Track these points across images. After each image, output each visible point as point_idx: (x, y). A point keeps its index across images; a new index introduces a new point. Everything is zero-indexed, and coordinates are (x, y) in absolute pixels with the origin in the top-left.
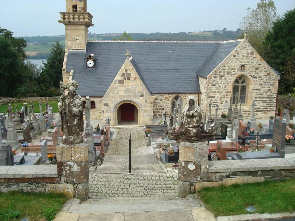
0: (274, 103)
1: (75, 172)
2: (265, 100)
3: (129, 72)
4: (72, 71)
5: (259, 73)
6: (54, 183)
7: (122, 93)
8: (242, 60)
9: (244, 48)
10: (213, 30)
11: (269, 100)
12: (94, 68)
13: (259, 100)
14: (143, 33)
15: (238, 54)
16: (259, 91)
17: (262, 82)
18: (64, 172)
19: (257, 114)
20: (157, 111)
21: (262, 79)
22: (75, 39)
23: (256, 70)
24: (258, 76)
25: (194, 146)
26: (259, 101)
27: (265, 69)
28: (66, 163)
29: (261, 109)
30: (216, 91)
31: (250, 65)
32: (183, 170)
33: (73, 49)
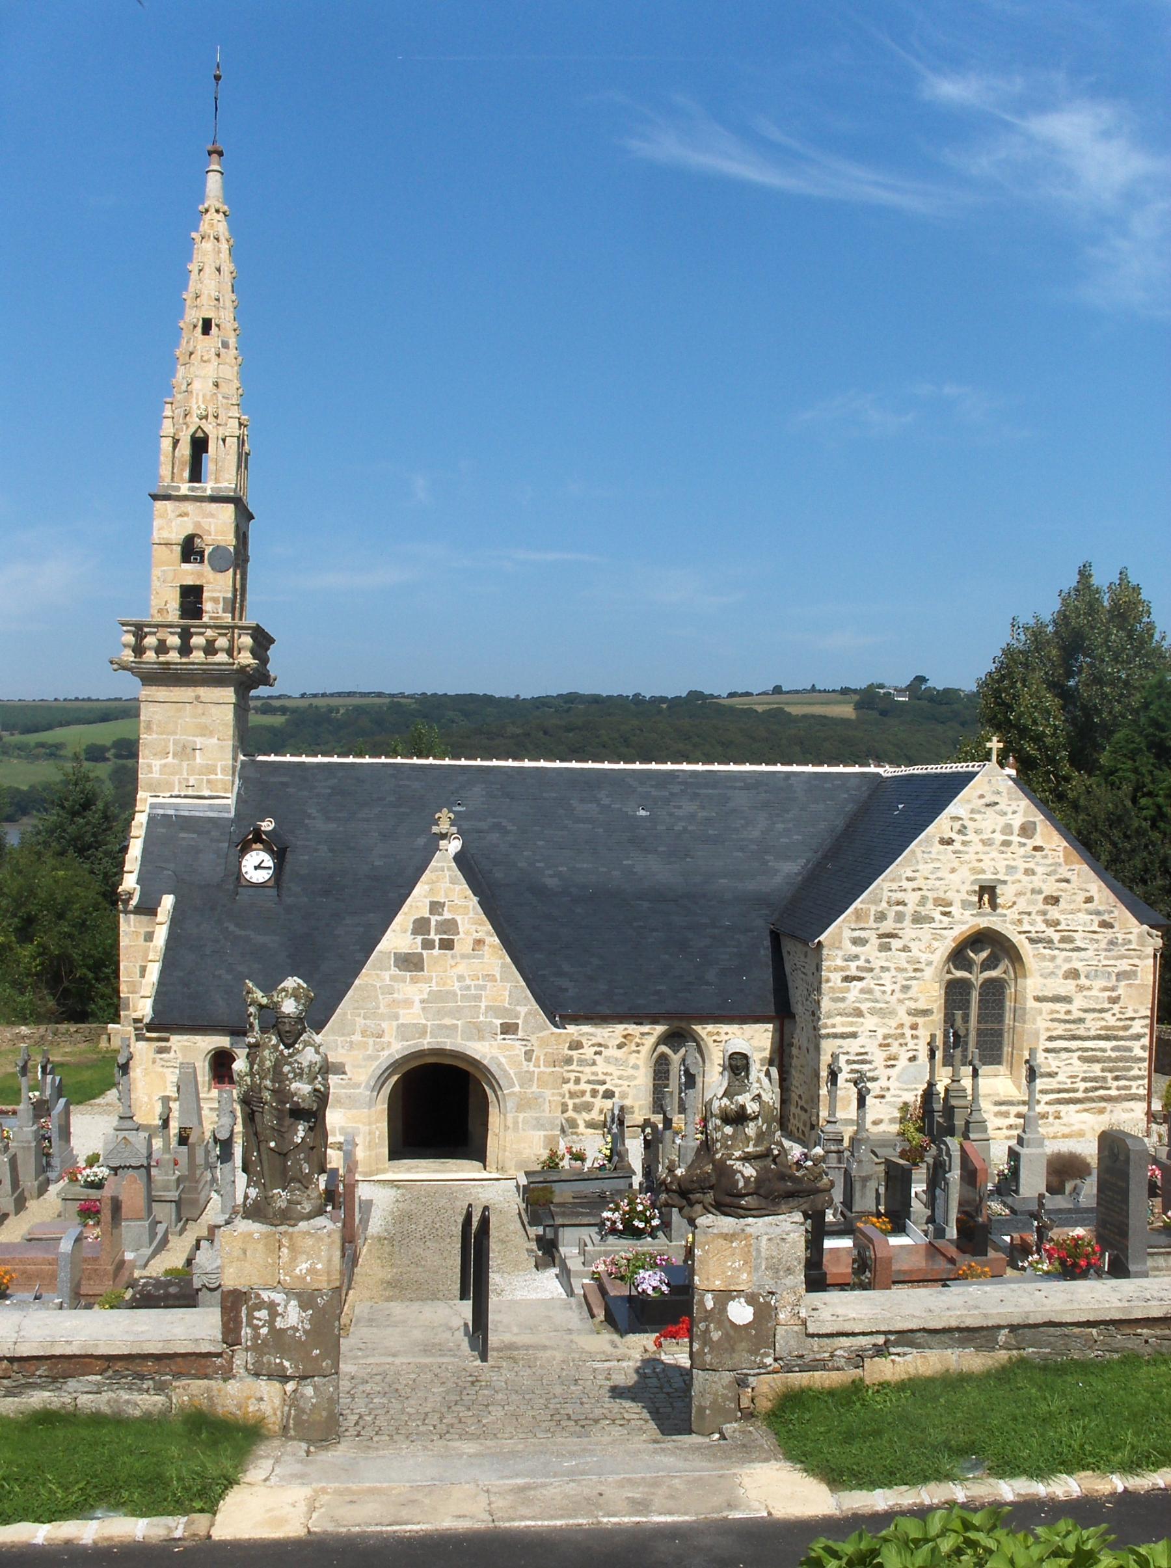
0: (1141, 1060)
1: (290, 1332)
2: (1093, 1050)
3: (447, 915)
4: (168, 901)
5: (1063, 923)
6: (206, 1377)
7: (413, 1015)
8: (981, 860)
9: (987, 805)
10: (859, 682)
11: (1113, 1049)
12: (273, 892)
13: (1067, 1050)
14: (498, 693)
15: (962, 831)
16: (1067, 1007)
17: (1078, 965)
18: (246, 1332)
19: (1058, 1117)
20: (577, 1101)
21: (1078, 949)
22: (184, 747)
23: (1049, 907)
24: (1056, 937)
25: (748, 1229)
26: (1064, 1055)
27: (1089, 900)
28: (258, 1296)
29: (1075, 1091)
30: (864, 1007)
31: (1017, 885)
32: (707, 1326)
33: (176, 793)
